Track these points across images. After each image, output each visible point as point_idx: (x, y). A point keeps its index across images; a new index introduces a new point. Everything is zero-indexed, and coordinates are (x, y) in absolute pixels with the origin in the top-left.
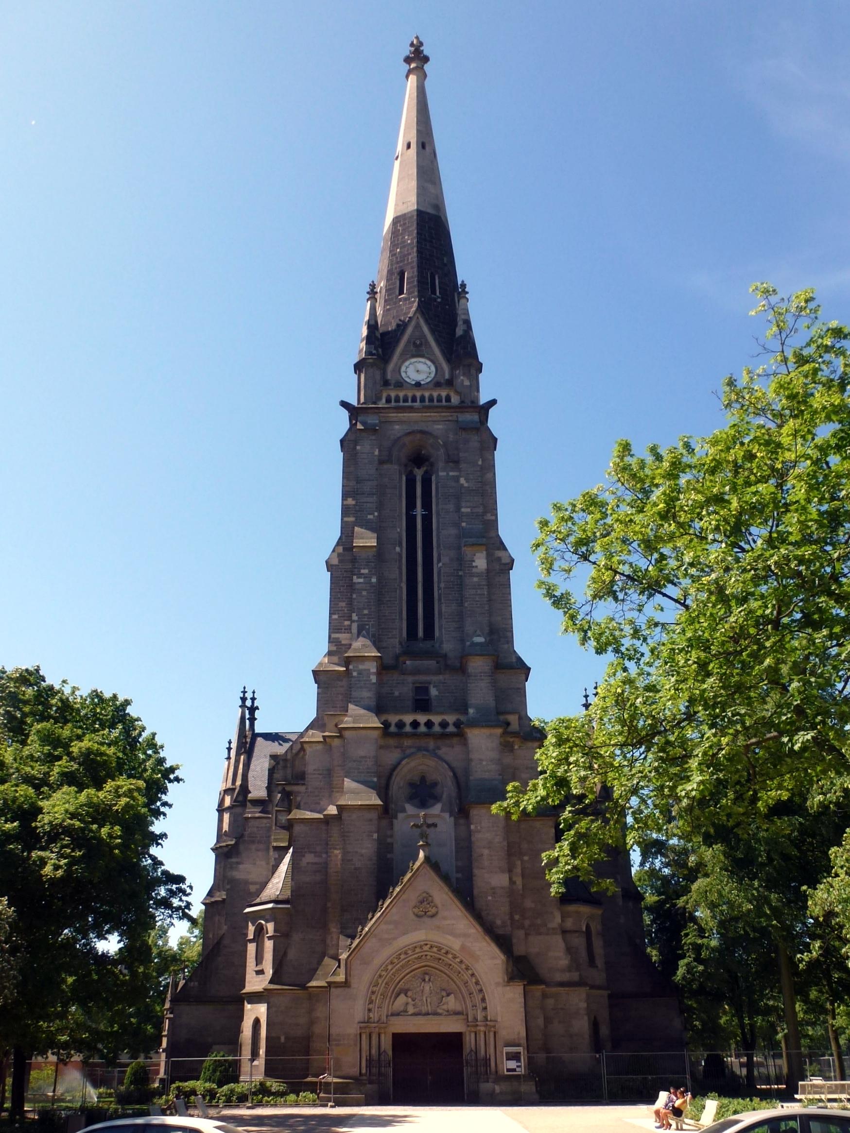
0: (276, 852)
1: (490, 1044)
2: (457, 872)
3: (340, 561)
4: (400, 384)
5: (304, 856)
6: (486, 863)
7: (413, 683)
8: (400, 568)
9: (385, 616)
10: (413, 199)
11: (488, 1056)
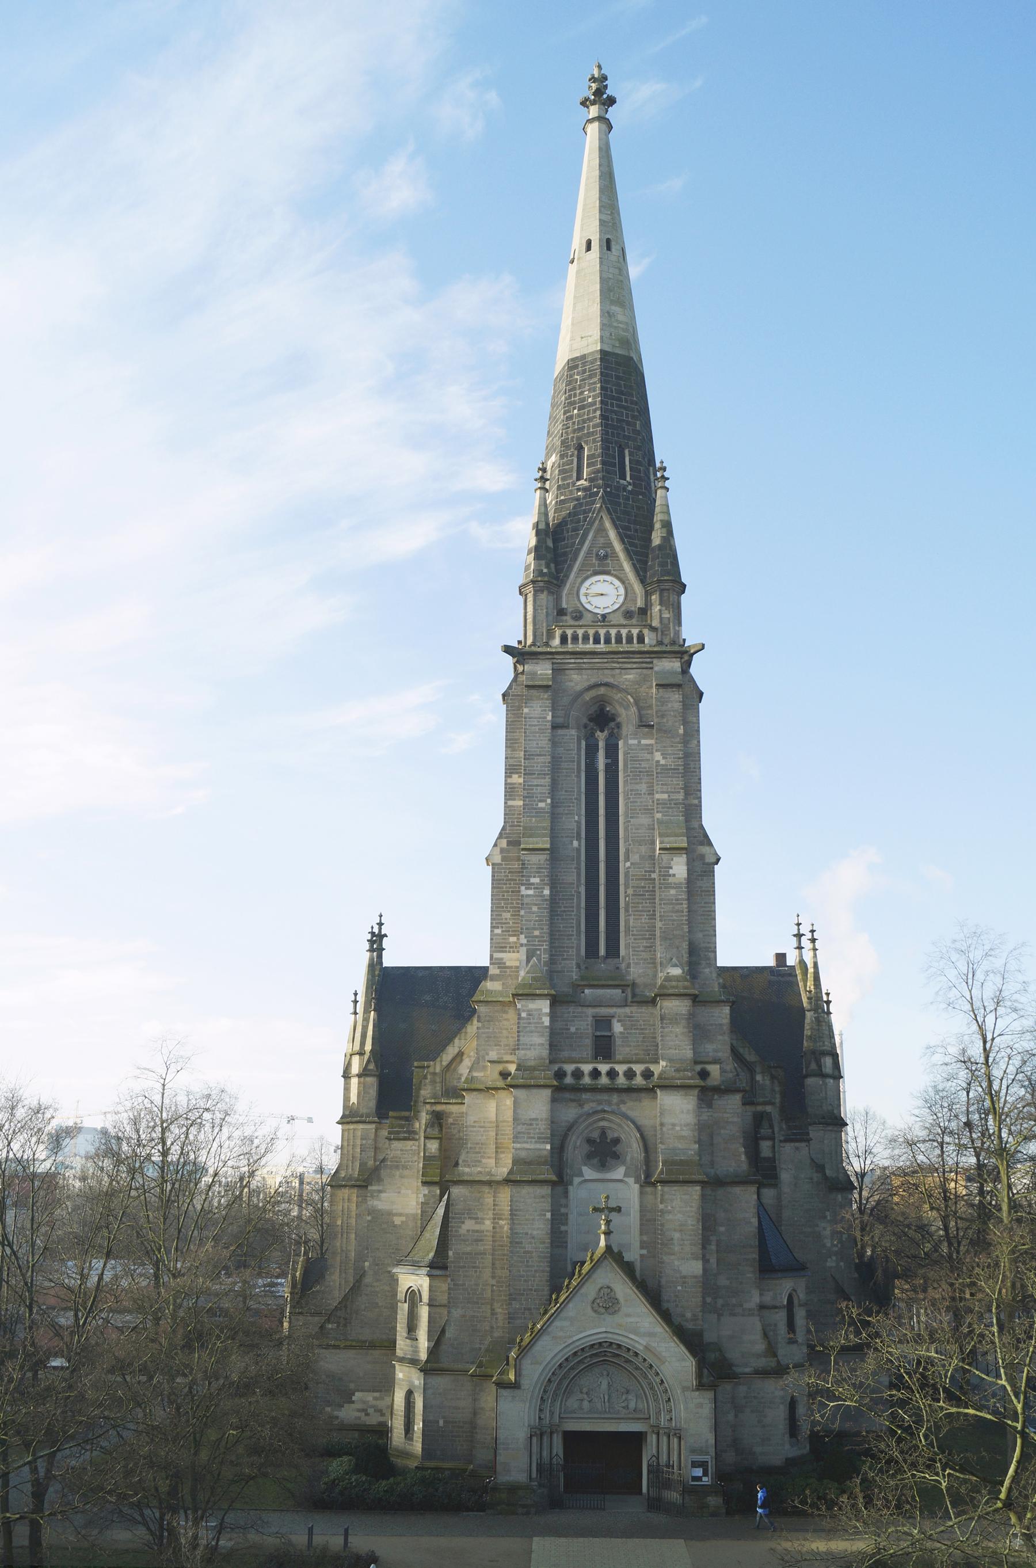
0: (425, 1188)
2: (642, 1248)
3: (503, 859)
4: (579, 615)
5: (463, 1223)
6: (677, 1249)
7: (593, 1017)
8: (578, 869)
9: (559, 931)
10: (595, 332)
11: (671, 1462)
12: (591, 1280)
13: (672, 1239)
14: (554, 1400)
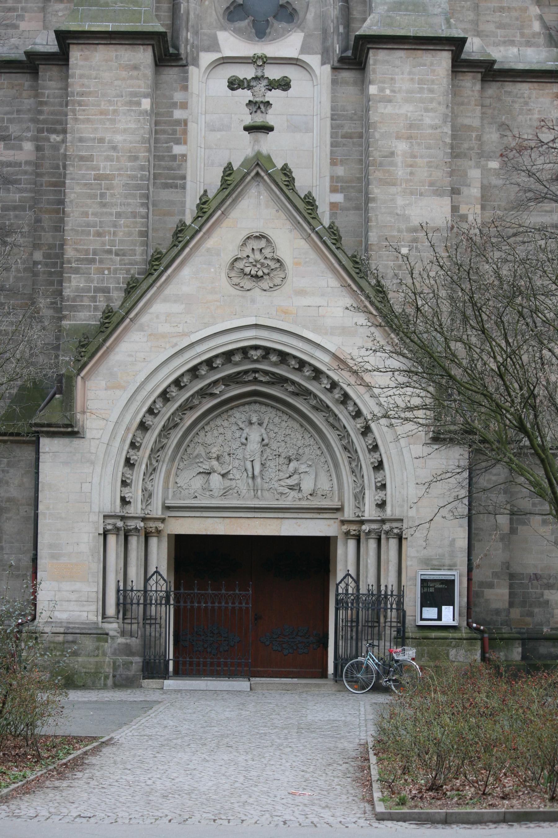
1: (388, 561)
2: (334, 190)
6: (401, 172)
12: (227, 223)
13: (392, 154)
14: (151, 471)
